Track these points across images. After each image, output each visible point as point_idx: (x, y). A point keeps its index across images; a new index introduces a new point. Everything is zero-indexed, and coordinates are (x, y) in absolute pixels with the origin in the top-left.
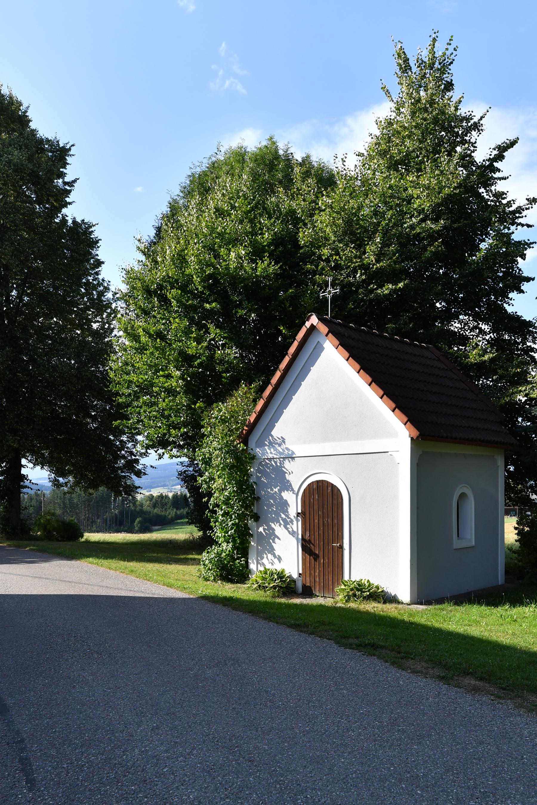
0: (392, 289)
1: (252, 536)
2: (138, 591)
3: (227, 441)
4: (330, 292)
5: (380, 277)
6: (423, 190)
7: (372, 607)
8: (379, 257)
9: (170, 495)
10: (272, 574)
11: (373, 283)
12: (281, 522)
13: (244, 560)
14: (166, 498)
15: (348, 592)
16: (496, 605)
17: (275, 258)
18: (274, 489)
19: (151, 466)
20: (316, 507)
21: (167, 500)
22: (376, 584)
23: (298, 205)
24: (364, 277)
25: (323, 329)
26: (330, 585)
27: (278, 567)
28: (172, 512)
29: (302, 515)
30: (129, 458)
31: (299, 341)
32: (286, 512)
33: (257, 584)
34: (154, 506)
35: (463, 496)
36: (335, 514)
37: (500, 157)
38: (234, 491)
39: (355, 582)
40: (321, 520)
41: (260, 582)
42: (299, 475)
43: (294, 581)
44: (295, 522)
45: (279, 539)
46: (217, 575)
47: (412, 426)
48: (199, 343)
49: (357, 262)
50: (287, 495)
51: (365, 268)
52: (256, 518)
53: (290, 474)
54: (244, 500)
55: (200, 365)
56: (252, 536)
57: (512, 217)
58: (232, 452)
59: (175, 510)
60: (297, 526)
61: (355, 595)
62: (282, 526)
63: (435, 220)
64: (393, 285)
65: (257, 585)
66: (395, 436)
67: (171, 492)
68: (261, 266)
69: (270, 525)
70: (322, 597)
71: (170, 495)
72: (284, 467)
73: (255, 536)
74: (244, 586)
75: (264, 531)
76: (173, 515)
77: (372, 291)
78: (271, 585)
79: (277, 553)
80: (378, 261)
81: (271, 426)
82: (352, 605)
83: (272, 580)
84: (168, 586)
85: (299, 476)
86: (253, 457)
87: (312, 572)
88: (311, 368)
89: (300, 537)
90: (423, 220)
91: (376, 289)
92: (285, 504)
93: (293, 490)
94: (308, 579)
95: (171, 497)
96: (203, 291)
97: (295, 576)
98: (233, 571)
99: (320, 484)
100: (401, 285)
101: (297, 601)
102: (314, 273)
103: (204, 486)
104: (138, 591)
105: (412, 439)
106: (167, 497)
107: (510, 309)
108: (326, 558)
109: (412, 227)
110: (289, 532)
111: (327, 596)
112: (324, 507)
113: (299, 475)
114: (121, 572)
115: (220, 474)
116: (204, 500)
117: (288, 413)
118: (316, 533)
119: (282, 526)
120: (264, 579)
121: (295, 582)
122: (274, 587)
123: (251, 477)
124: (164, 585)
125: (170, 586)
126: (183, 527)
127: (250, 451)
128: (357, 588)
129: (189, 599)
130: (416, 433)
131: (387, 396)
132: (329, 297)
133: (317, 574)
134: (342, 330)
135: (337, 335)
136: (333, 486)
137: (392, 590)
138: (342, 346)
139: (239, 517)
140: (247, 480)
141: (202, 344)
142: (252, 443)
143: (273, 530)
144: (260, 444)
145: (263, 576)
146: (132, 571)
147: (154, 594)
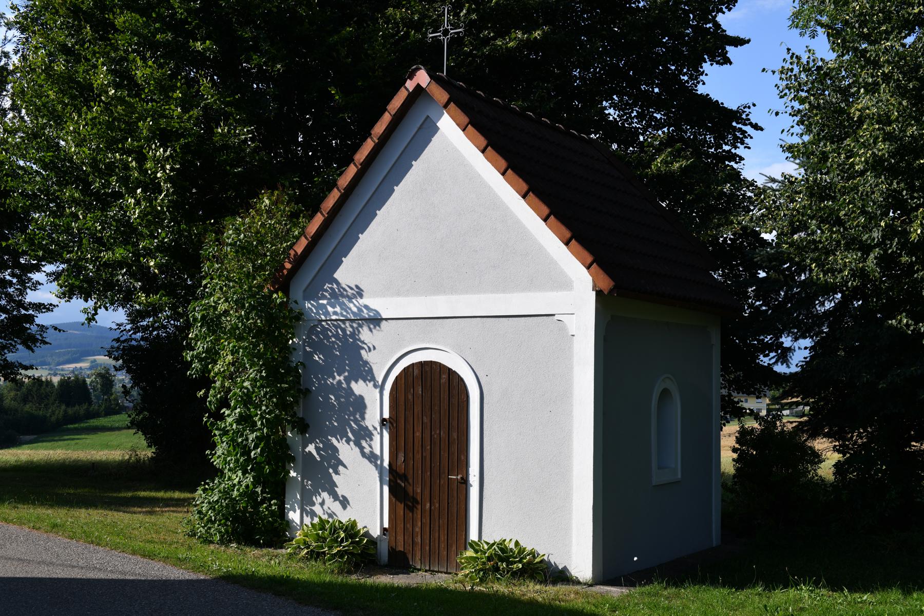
0: (521, 40)
1: (293, 459)
2: (88, 568)
3: (250, 288)
4: (446, 33)
7: (532, 590)
9: (56, 380)
10: (335, 531)
11: (487, 28)
12: (350, 435)
13: (275, 504)
14: (47, 386)
15: (484, 563)
16: (740, 585)
18: (338, 378)
19: (56, 329)
20: (418, 409)
21: (48, 390)
22: (529, 549)
24: (474, 17)
25: (440, 95)
26: (442, 549)
27: (344, 517)
28: (58, 411)
30: (15, 313)
31: (393, 113)
33: (308, 548)
34: (25, 399)
35: (665, 393)
36: (455, 423)
38: (261, 377)
39: (493, 544)
40: (427, 432)
41: (314, 544)
44: (377, 438)
45: (345, 467)
46: (227, 531)
47: (601, 272)
48: (185, 110)
52: (302, 427)
53: (370, 350)
54: (282, 394)
56: (293, 459)
58: (264, 306)
59: (63, 407)
60: (381, 443)
61: (496, 569)
62: (352, 443)
64: (523, 34)
65: (306, 551)
66: (568, 290)
67: (55, 375)
69: (330, 440)
70: (426, 571)
71: (56, 380)
72: (359, 340)
73: (300, 460)
74: (279, 551)
75: (318, 453)
76: (60, 416)
77: (486, 41)
78: (335, 551)
79: (340, 491)
81: (335, 262)
82: (501, 588)
83: (335, 540)
84: (144, 556)
85: (387, 355)
86: (299, 316)
87: (409, 526)
88: (414, 163)
89: (386, 463)
91: (494, 38)
92: (360, 405)
93: (373, 379)
94: (400, 538)
95: (56, 384)
96: (186, 18)
97: (376, 532)
98: (258, 524)
99: (428, 369)
100: (537, 34)
101: (384, 580)
103: (196, 365)
104: (88, 568)
105: (599, 294)
106: (49, 383)
108: (436, 501)
110: (363, 455)
111: (436, 569)
113: (387, 354)
114: (34, 528)
115: (234, 347)
116: (332, 397)
117: (367, 241)
118: (418, 456)
119: (352, 443)
120: (319, 538)
121: (376, 543)
122: (341, 554)
123: (294, 353)
124: (134, 553)
125: (150, 556)
126: (83, 436)
127: (293, 305)
128: (499, 555)
129: (199, 581)
130: (606, 284)
131: (555, 216)
133: (418, 529)
136: (451, 373)
137: (558, 561)
138: (473, 125)
139: (269, 424)
140: (286, 359)
141: (191, 113)
142: (297, 291)
143: (336, 450)
144: (313, 293)
145: (318, 534)
146: (55, 526)
147: (134, 574)
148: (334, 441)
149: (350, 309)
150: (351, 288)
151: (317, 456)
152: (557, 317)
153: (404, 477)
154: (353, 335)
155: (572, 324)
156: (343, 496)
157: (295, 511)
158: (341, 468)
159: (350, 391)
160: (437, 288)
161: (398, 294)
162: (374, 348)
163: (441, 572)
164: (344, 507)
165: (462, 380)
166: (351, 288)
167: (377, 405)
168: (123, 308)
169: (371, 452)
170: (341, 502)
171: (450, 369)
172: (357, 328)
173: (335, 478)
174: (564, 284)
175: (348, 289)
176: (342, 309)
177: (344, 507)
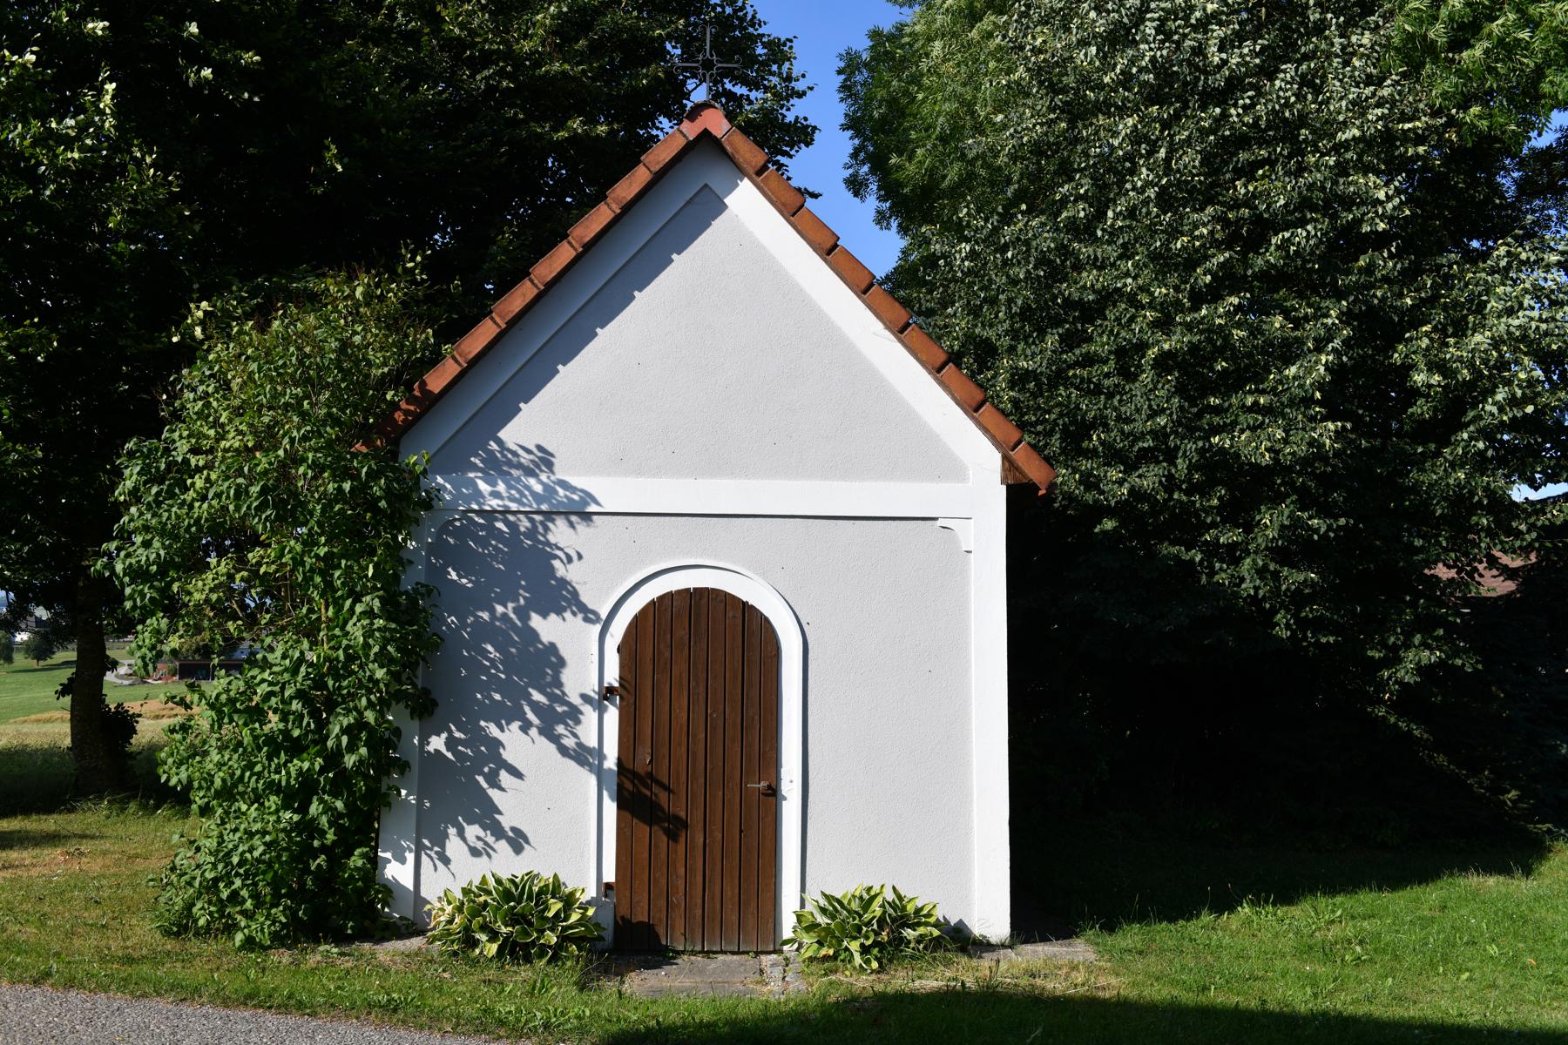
12: (531, 716)
60: (604, 731)
62: (534, 732)
66: (961, 480)
72: (548, 544)
79: (506, 821)
89: (611, 763)
92: (549, 662)
110: (564, 751)
113: (612, 578)
117: (571, 378)
148: (493, 730)
149: (528, 488)
150: (529, 451)
151: (449, 755)
152: (939, 523)
153: (650, 778)
154: (532, 533)
155: (967, 536)
156: (513, 829)
157: (403, 861)
158: (504, 776)
159: (534, 635)
160: (714, 466)
161: (639, 472)
162: (580, 557)
163: (725, 953)
164: (518, 850)
165: (767, 620)
166: (529, 451)
167: (588, 657)
168: (903, 230)
169: (580, 745)
170: (510, 841)
171: (745, 604)
172: (542, 523)
173: (493, 793)
174: (950, 469)
175: (521, 452)
176: (509, 487)
177: (518, 850)
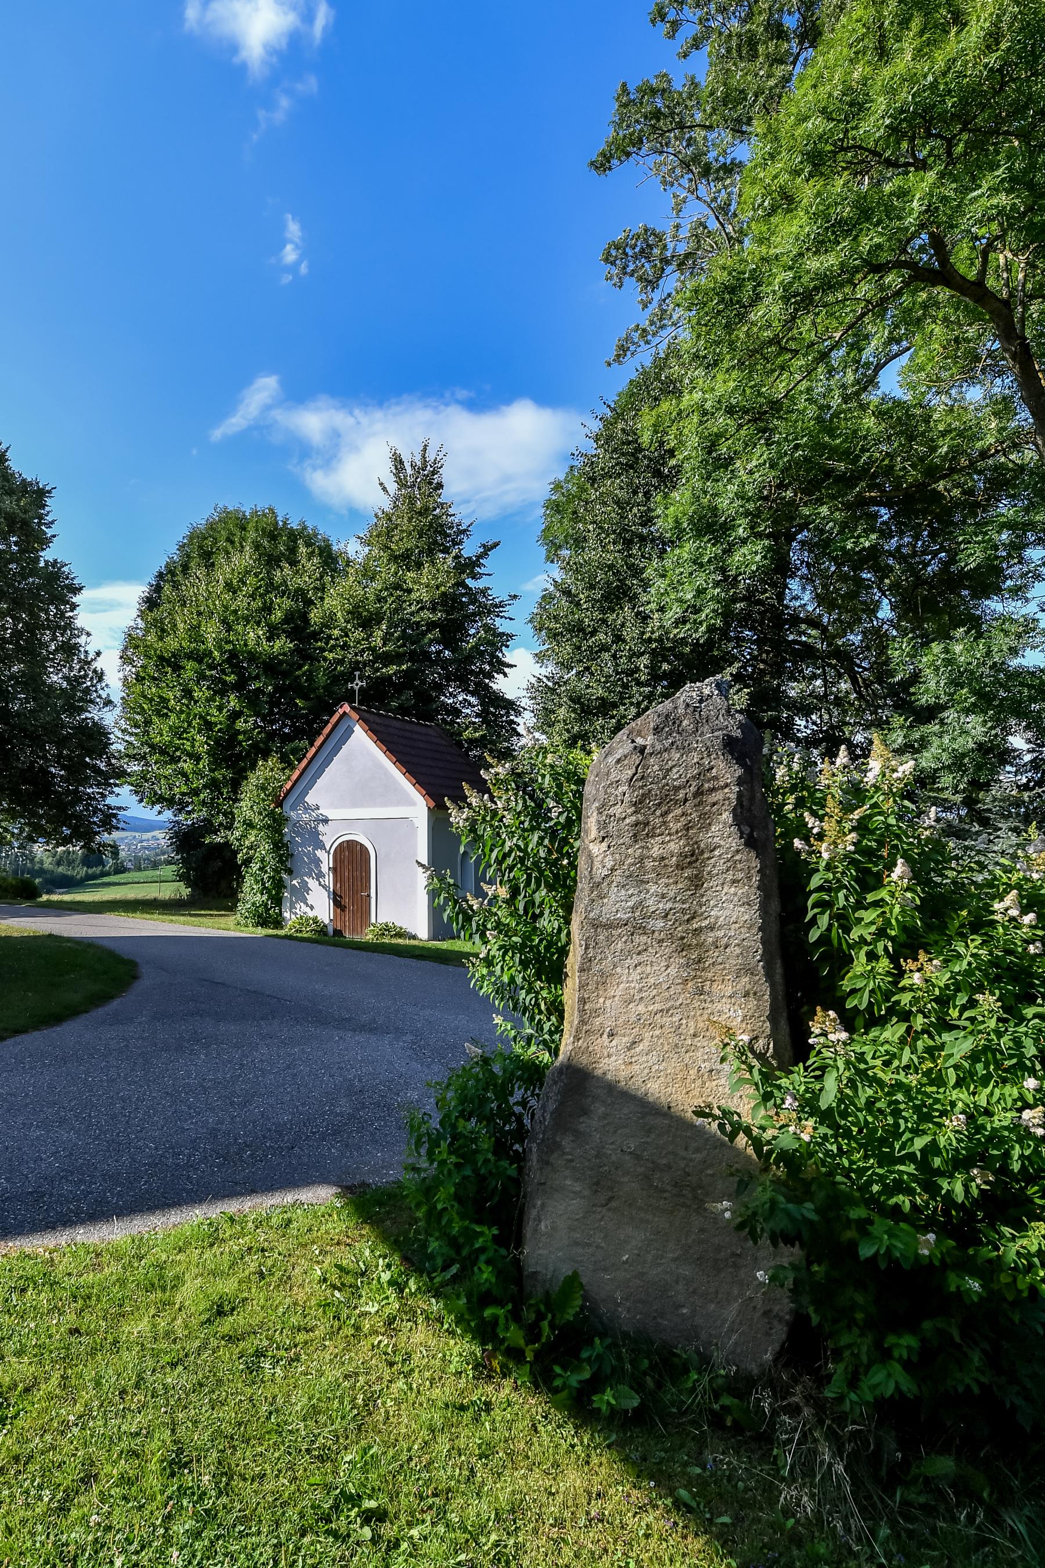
5: (387, 659)
6: (424, 584)
8: (385, 641)
17: (291, 635)
23: (303, 581)
25: (355, 716)
27: (311, 914)
29: (334, 869)
32: (318, 866)
37: (484, 554)
42: (331, 837)
43: (325, 926)
49: (365, 645)
50: (320, 854)
51: (373, 649)
55: (220, 730)
57: (495, 609)
60: (329, 880)
63: (433, 610)
68: (278, 644)
77: (378, 670)
80: (384, 645)
90: (422, 609)
92: (318, 862)
97: (327, 922)
98: (269, 918)
100: (404, 667)
102: (323, 650)
107: (495, 687)
109: (412, 614)
112: (353, 862)
132: (357, 688)
134: (366, 715)
135: (365, 721)
